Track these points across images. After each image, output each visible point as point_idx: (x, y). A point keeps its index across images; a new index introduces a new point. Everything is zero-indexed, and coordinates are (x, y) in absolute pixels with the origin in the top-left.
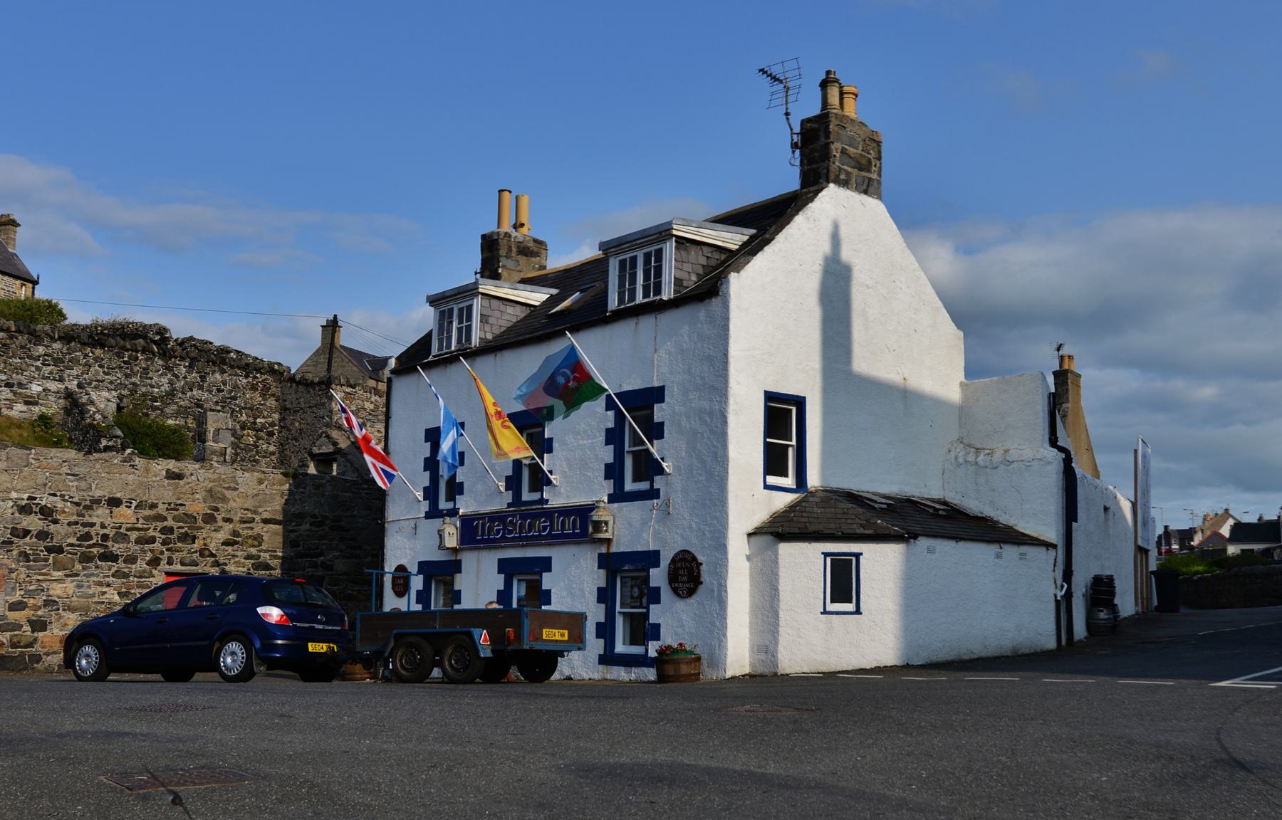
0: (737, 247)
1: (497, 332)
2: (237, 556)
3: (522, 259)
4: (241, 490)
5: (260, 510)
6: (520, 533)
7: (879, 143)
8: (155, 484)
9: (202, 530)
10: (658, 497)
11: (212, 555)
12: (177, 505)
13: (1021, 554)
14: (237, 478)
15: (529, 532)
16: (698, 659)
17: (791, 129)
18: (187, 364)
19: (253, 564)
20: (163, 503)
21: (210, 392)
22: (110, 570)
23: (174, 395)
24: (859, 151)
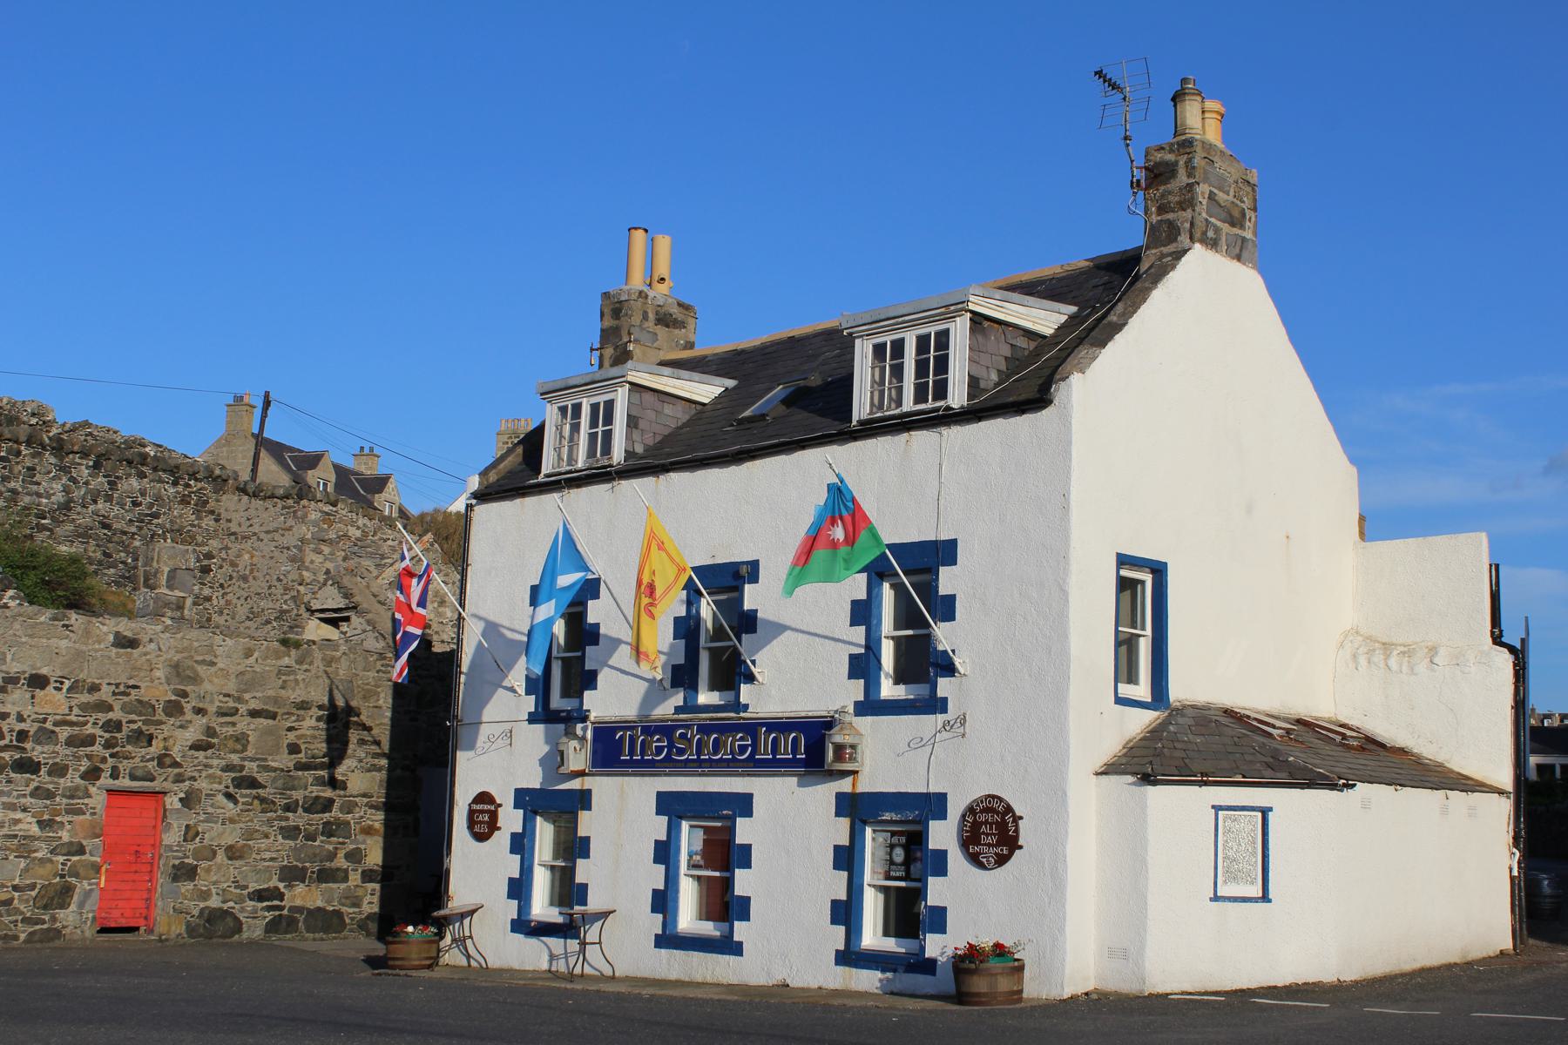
0: (1052, 331)
1: (650, 442)
2: (211, 767)
3: (661, 331)
4: (220, 665)
5: (247, 696)
6: (699, 753)
8: (99, 654)
9: (163, 727)
10: (944, 710)
11: (176, 764)
12: (129, 687)
13: (1470, 808)
14: (215, 648)
15: (716, 752)
16: (1021, 968)
18: (91, 463)
19: (233, 780)
20: (109, 684)
21: (122, 505)
22: (28, 786)
23: (70, 509)
24: (1231, 198)
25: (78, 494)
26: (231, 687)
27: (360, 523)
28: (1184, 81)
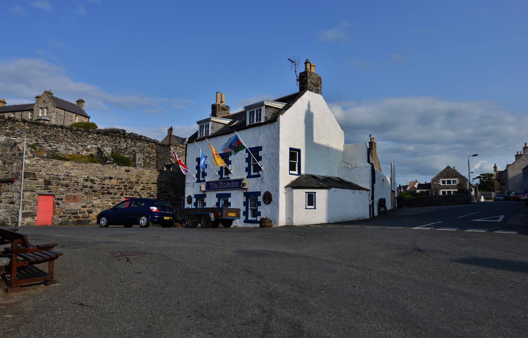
0: (282, 108)
1: (216, 131)
2: (144, 193)
3: (223, 111)
5: (151, 180)
7: (321, 79)
10: (260, 177)
11: (138, 193)
13: (360, 192)
15: (225, 186)
17: (297, 76)
21: (137, 148)
24: (315, 82)
25: (129, 146)
26: (148, 179)
27: (182, 150)
28: (307, 60)
